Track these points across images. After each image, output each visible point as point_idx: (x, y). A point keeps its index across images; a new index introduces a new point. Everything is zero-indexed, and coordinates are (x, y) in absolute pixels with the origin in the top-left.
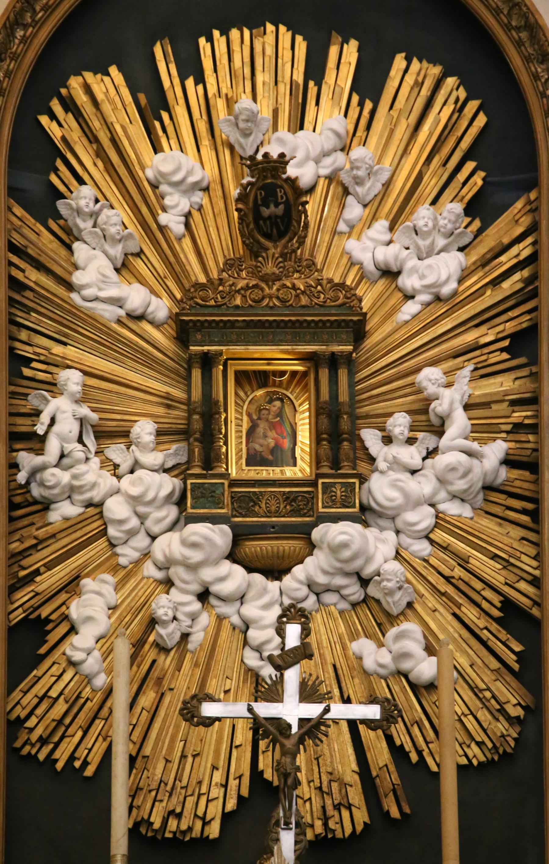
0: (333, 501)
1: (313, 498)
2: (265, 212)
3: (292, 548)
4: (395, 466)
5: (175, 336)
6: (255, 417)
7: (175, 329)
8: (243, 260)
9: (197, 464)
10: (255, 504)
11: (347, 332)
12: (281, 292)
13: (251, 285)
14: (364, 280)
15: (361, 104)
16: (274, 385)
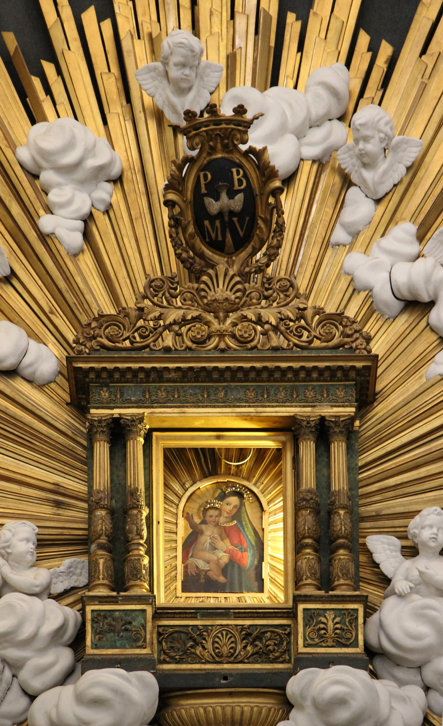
0: (321, 636)
1: (289, 634)
2: (213, 206)
3: (255, 709)
4: (422, 588)
5: (69, 400)
6: (197, 520)
7: (68, 390)
8: (176, 280)
9: (101, 581)
10: (197, 643)
11: (346, 386)
12: (239, 327)
13: (189, 317)
14: (375, 316)
15: (373, 48)
16: (228, 472)
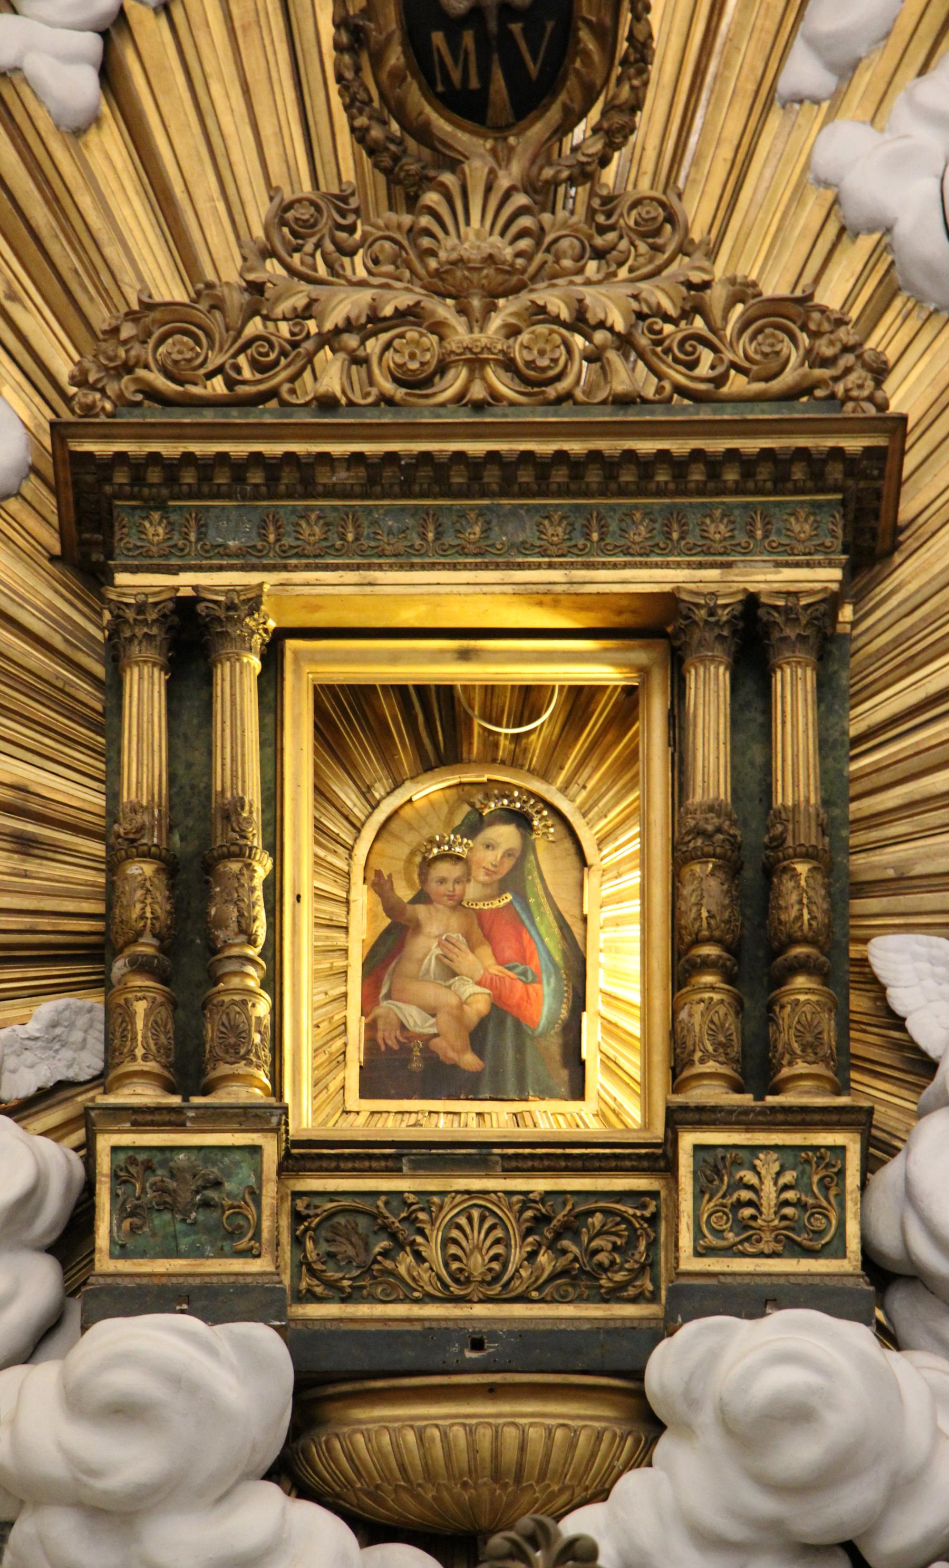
1: (653, 1220)
3: (559, 1434)
5: (57, 549)
6: (404, 893)
7: (55, 520)
8: (354, 203)
9: (140, 1065)
11: (817, 507)
12: (525, 337)
13: (388, 311)
14: (898, 303)
16: (490, 757)
